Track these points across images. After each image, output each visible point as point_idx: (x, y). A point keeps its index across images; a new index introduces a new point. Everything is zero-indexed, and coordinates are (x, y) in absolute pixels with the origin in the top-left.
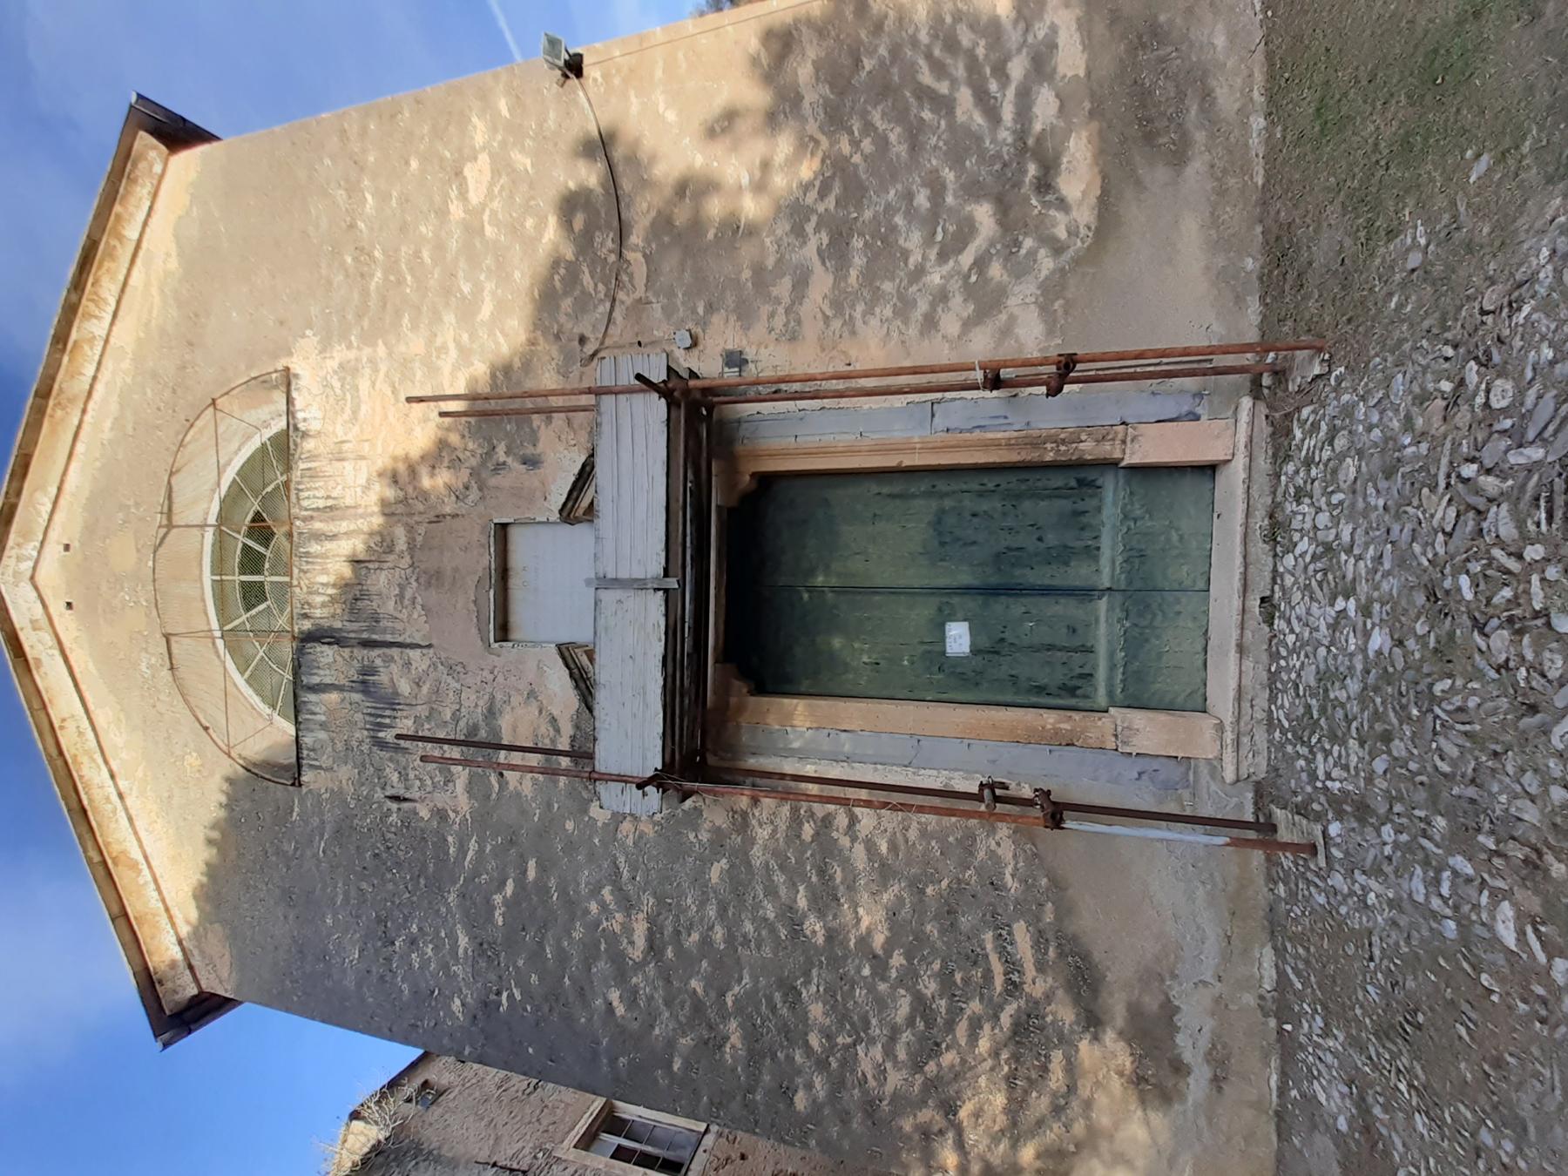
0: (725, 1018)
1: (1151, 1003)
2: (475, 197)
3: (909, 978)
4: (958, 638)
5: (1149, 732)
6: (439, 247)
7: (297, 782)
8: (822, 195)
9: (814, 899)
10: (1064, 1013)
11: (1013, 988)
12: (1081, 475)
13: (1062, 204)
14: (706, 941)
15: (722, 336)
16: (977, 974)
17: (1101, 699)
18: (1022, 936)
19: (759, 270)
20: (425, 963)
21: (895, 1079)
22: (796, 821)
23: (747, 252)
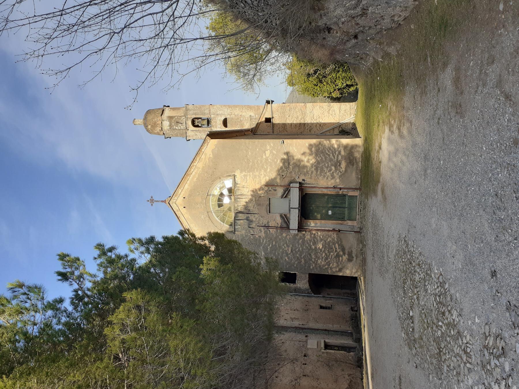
0: (301, 258)
1: (350, 251)
2: (267, 155)
4: (330, 212)
5: (350, 223)
6: (261, 161)
10: (341, 253)
11: (336, 251)
12: (344, 196)
14: (299, 250)
15: (302, 177)
19: (445, 359)
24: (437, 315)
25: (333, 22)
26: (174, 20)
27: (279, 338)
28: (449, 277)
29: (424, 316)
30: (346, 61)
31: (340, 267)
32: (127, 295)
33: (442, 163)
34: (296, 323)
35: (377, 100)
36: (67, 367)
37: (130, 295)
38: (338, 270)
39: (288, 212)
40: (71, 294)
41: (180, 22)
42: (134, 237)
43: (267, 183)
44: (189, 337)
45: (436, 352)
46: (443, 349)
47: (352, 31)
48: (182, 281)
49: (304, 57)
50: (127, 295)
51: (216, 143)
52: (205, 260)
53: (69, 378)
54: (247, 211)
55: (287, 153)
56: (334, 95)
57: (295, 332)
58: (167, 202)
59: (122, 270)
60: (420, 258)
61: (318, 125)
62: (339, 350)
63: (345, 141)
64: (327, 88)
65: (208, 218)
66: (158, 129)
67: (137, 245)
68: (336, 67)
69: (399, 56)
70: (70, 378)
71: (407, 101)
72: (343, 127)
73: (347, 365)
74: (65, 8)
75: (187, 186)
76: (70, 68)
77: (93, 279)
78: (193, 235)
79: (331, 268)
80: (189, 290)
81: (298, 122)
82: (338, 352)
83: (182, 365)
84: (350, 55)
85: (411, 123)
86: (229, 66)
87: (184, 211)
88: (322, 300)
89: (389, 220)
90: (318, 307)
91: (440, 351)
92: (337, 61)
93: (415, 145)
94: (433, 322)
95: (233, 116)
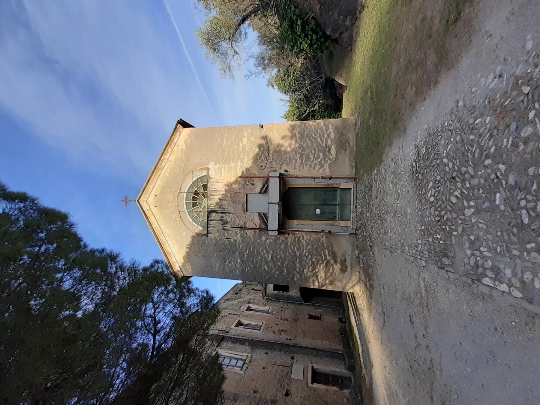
0: (284, 268)
2: (244, 144)
3: (311, 259)
5: (342, 223)
7: (207, 236)
8: (299, 149)
9: (297, 249)
10: (332, 262)
11: (326, 259)
12: (335, 189)
13: (331, 154)
14: (281, 257)
15: (284, 167)
16: (320, 258)
17: (337, 219)
18: (327, 251)
20: (232, 265)
21: (309, 274)
22: (295, 238)
23: (288, 155)
34: (283, 338)
51: (189, 132)
55: (265, 138)
65: (179, 218)
87: (155, 210)
88: (312, 308)
90: (307, 316)
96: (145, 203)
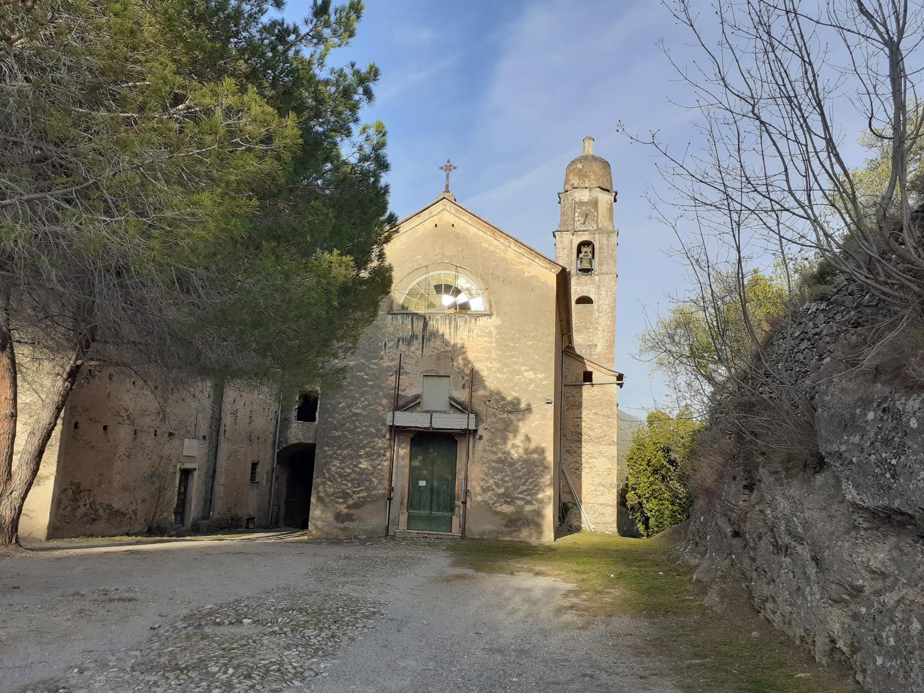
4: (422, 483)
5: (404, 518)
6: (516, 363)
10: (350, 502)
11: (354, 492)
12: (452, 510)
14: (358, 427)
15: (486, 435)
18: (365, 494)
19: (168, 678)
24: (247, 665)
25: (765, 493)
26: (773, 210)
27: (204, 389)
28: (313, 687)
29: (243, 642)
30: (692, 518)
31: (327, 500)
32: (291, 119)
33: (514, 679)
34: (227, 420)
35: (623, 569)
36: (166, 12)
37: (291, 125)
38: (321, 495)
39: (425, 409)
40: (289, 22)
41: (772, 222)
42: (388, 134)
43: (477, 372)
44: (217, 227)
45: (180, 663)
46: (186, 674)
47: (747, 527)
48: (310, 218)
49: (699, 443)
50: (291, 119)
51: (549, 283)
52: (348, 259)
53: (148, 15)
54: (428, 336)
56: (630, 495)
57: (212, 418)
58: (446, 195)
59: (332, 112)
60: (345, 638)
61: (577, 465)
62: (179, 493)
63: (549, 513)
64: (644, 483)
65: (416, 266)
66: (575, 181)
67: (375, 139)
68: (680, 499)
69: (703, 610)
70: (149, 18)
71: (623, 622)
72: (575, 511)
73: (154, 509)
74: (801, 19)
75: (474, 230)
76: (692, 25)
77: (315, 61)
78: (387, 240)
79: (324, 483)
80: (294, 229)
81: (584, 430)
82: (176, 493)
83: (168, 214)
84: (704, 524)
85: (583, 628)
86: (689, 307)
87: (430, 224)
88: (268, 467)
89: (410, 586)
90: (255, 459)
91: (182, 671)
92: (692, 502)
93: (545, 633)
94: (232, 658)
95: (596, 314)
96: (442, 207)
